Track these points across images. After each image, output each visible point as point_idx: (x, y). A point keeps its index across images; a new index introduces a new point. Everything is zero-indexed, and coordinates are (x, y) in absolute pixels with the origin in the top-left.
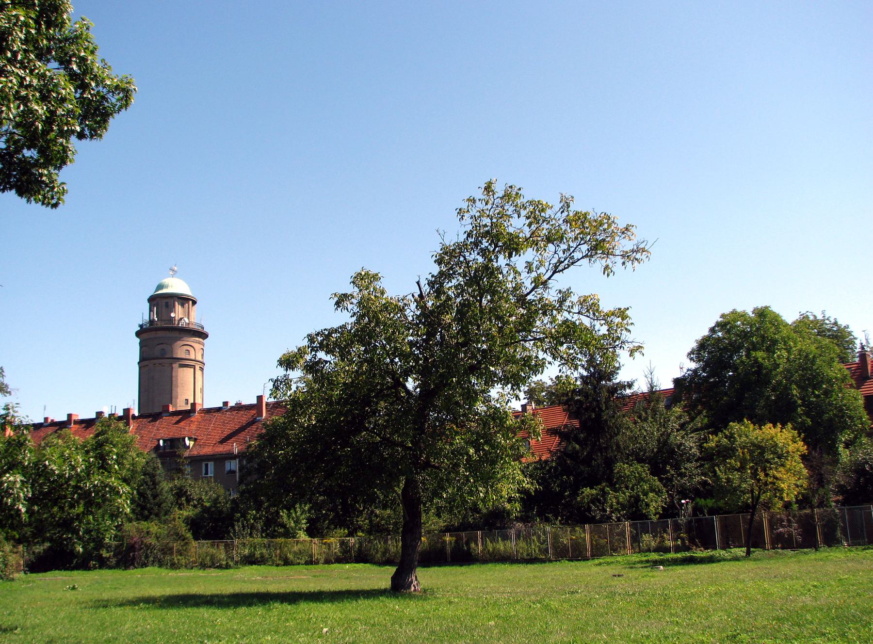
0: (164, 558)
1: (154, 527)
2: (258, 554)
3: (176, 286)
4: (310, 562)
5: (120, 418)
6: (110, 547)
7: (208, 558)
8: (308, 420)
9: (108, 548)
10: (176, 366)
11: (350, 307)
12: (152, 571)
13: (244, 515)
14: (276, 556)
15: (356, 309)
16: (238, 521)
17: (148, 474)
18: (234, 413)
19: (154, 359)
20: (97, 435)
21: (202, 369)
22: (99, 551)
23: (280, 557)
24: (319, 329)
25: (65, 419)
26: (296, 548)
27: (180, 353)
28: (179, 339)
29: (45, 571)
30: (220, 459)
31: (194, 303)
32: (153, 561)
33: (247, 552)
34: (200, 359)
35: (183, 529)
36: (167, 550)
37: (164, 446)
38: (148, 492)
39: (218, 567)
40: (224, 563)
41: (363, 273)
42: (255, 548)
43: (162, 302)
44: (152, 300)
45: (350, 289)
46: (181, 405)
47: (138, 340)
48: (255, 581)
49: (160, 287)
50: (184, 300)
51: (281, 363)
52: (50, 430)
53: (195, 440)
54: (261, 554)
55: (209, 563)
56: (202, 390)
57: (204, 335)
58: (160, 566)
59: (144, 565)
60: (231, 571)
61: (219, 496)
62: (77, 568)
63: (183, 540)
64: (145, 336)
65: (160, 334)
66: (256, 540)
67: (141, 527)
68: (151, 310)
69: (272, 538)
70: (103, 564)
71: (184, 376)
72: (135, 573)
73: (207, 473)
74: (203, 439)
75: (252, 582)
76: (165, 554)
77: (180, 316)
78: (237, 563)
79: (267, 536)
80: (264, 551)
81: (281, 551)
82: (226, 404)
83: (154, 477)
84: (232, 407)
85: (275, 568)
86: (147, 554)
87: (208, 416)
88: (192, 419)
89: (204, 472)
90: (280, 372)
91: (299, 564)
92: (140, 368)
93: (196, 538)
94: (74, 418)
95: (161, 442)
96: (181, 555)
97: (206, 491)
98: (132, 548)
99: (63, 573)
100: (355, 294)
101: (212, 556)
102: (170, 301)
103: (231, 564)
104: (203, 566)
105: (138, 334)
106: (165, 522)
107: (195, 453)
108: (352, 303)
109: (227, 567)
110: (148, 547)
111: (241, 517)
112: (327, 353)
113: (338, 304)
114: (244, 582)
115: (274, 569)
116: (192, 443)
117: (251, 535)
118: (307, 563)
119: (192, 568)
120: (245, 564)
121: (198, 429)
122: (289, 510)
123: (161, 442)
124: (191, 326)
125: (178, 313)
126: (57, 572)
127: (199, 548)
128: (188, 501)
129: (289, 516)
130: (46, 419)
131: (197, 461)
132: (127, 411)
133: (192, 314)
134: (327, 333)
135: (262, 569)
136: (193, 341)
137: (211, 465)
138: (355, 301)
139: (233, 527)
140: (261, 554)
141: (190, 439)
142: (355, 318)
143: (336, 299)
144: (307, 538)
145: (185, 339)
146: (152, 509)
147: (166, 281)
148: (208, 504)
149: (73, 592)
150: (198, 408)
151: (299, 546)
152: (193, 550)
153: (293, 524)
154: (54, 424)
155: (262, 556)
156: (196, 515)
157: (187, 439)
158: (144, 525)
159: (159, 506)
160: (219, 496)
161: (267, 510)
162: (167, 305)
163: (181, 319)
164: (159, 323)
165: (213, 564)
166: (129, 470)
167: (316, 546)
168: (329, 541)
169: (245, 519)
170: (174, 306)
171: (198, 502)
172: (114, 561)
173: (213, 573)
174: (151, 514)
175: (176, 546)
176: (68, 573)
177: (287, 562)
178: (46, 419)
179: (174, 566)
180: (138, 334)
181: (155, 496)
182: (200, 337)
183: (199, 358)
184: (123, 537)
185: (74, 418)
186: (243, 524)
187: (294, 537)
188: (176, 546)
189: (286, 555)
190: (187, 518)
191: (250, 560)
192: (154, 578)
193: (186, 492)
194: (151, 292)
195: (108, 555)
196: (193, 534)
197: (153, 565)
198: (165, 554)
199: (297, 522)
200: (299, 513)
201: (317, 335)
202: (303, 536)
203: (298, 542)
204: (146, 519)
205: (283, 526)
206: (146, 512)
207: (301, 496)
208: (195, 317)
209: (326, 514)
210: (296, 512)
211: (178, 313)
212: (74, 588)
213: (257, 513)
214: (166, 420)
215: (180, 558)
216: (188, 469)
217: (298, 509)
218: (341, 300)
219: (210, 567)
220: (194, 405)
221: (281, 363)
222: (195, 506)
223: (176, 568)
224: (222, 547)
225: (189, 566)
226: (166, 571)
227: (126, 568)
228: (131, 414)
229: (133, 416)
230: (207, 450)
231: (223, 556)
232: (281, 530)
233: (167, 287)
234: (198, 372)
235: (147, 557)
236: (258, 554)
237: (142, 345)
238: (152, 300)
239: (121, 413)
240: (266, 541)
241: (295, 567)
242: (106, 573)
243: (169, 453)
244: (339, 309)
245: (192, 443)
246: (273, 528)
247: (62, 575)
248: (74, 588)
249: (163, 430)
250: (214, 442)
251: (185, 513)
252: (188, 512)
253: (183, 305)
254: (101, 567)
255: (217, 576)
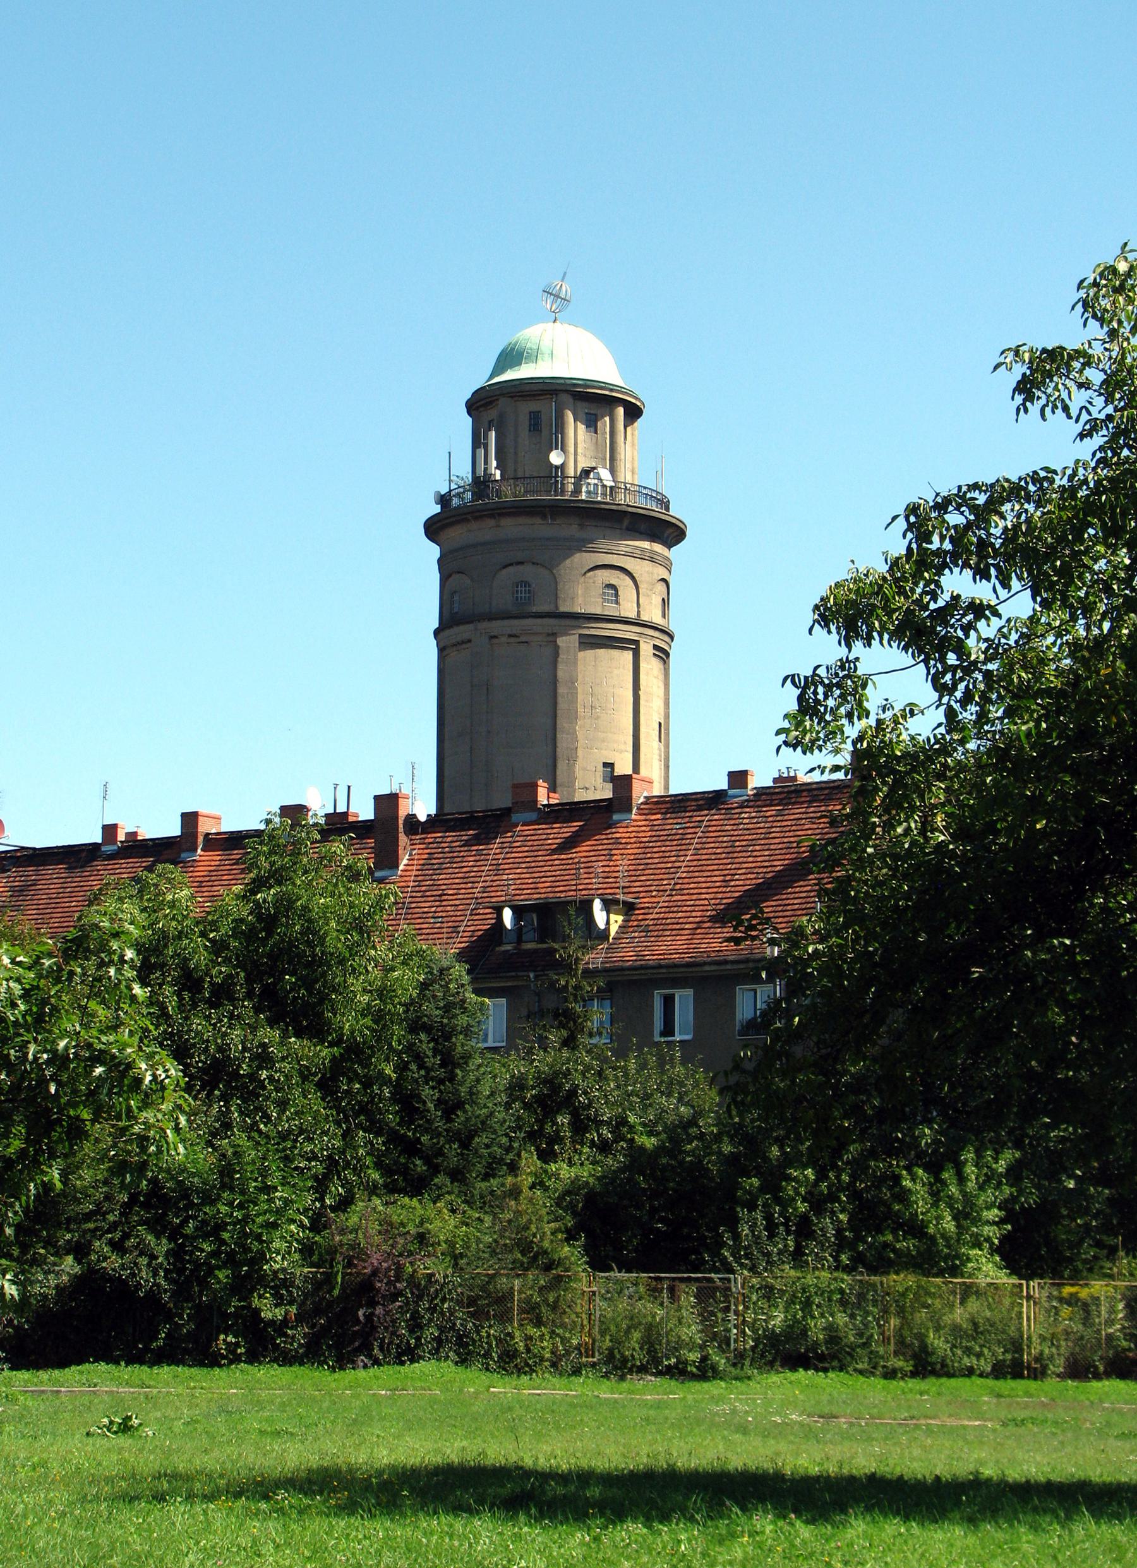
0: (478, 1329)
1: (442, 1218)
2: (816, 1328)
3: (568, 352)
4: (1015, 1367)
5: (363, 829)
6: (287, 1284)
7: (636, 1335)
8: (931, 825)
9: (280, 1287)
10: (567, 642)
11: (1079, 398)
12: (433, 1376)
13: (774, 1180)
14: (886, 1341)
15: (1100, 408)
16: (752, 1207)
17: (427, 1029)
18: (771, 811)
19: (491, 617)
20: (259, 884)
21: (662, 654)
22: (246, 1298)
23: (901, 1343)
24: (947, 487)
25: (174, 829)
26: (959, 1315)
27: (584, 596)
28: (581, 545)
29: (63, 1364)
30: (713, 980)
31: (634, 412)
32: (439, 1341)
33: (778, 1319)
34: (656, 618)
35: (546, 1232)
36: (488, 1303)
37: (518, 930)
38: (426, 1092)
39: (669, 1372)
40: (694, 1356)
41: (1123, 267)
42: (807, 1304)
43: (517, 410)
44: (482, 405)
45: (1074, 332)
46: (591, 787)
47: (434, 551)
48: (780, 1431)
49: (510, 356)
50: (596, 402)
51: (825, 615)
52: (126, 868)
53: (629, 909)
54: (830, 1328)
55: (640, 1357)
56: (663, 729)
57: (669, 532)
58: (464, 1361)
59: (408, 1354)
60: (715, 1388)
61: (699, 1113)
62: (169, 1356)
63: (548, 1268)
64: (457, 534)
65: (511, 527)
66: (810, 1280)
67: (397, 1215)
68: (478, 442)
69: (873, 1270)
70: (261, 1344)
71: (601, 681)
72: (368, 1382)
73: (668, 1030)
74: (655, 903)
75: (770, 1432)
76: (479, 1315)
77: (583, 463)
78: (740, 1356)
79: (858, 1260)
80: (841, 1319)
81: (906, 1323)
82: (738, 778)
83: (448, 1038)
84: (761, 792)
85: (878, 1383)
86: (416, 1316)
87: (674, 824)
88: (620, 833)
89: (658, 1024)
90: (827, 649)
91: (970, 1372)
92: (441, 650)
93: (598, 1264)
94: (205, 827)
95: (507, 915)
96: (538, 1322)
97: (656, 1093)
98: (364, 1290)
99: (126, 1372)
100: (1097, 350)
101: (650, 1327)
102: (547, 408)
103: (720, 1361)
104: (618, 1366)
105: (433, 529)
106: (489, 1203)
107: (627, 955)
108: (1084, 385)
109: (705, 1372)
110: (421, 1288)
111: (763, 1189)
112: (982, 573)
113: (1026, 388)
114: (744, 1429)
115: (875, 1389)
116: (617, 920)
117: (797, 1257)
118: (999, 1371)
119: (577, 1372)
120: (771, 1364)
121: (639, 868)
122: (934, 1169)
123: (507, 915)
124: (621, 498)
125: (576, 449)
126: (102, 1366)
127: (603, 1298)
128: (580, 1127)
129: (936, 1194)
130: (110, 830)
131: (630, 986)
132: (387, 803)
133: (628, 452)
134: (982, 499)
135: (829, 1386)
136: (630, 551)
137: (684, 998)
138: (1096, 377)
139: (733, 1223)
140: (830, 1328)
141: (609, 905)
142: (1098, 440)
143: (1020, 370)
144: (1004, 1279)
145: (603, 544)
146: (440, 1153)
147: (533, 335)
148: (649, 1142)
149: (123, 1441)
150: (639, 794)
151: (973, 1305)
152: (581, 1305)
153: (949, 1225)
154: (137, 847)
155: (833, 1336)
156: (609, 1180)
157: (597, 904)
158: (409, 1210)
159: (465, 1144)
160: (699, 1113)
161: (859, 1167)
162: (535, 423)
163: (586, 473)
164: (507, 489)
165: (656, 1361)
166: (366, 1011)
167: (1035, 1311)
168: (1084, 1294)
169: (778, 1200)
170: (561, 427)
171: (615, 1131)
172: (299, 1335)
173: (651, 1390)
174: (435, 1170)
175: (521, 1287)
176: (141, 1372)
177: (925, 1365)
178: (110, 830)
179: (512, 1362)
180: (433, 529)
181: (450, 1107)
182: (653, 537)
183: (653, 614)
184: (332, 1251)
185: (205, 827)
186: (769, 1217)
187: (954, 1271)
188: (521, 1287)
189: (921, 1338)
190: (574, 1188)
191: (790, 1352)
192: (433, 1401)
193: (573, 1093)
194: (478, 378)
195: (279, 1313)
196: (588, 1249)
197: (436, 1353)
198: (479, 1315)
199: (965, 1215)
200: (971, 1185)
201: (942, 506)
202: (987, 1270)
203: (968, 1291)
204: (416, 1187)
205: (916, 1229)
206: (419, 1165)
207: (969, 1124)
208: (639, 464)
209: (1079, 1191)
210: (962, 1179)
211: (576, 449)
212: (126, 1427)
213: (821, 1176)
214: (526, 835)
215: (532, 1331)
216: (598, 1015)
217: (970, 1170)
218: (1041, 374)
219: (642, 1369)
220: (623, 784)
221: (825, 615)
222: (604, 1147)
223: (520, 1371)
224: (688, 1298)
225: (566, 1364)
226: (485, 1378)
227: (343, 1361)
228: (402, 814)
229: (411, 819)
230: (670, 948)
231: (692, 1331)
232: (907, 1244)
233: (533, 356)
234: (650, 666)
235: (416, 1326)
236: (816, 1328)
237: (449, 568)
238: (482, 405)
239: (365, 811)
240: (846, 1281)
241: (953, 1382)
242: (269, 1377)
243: (527, 957)
244: (1034, 408)
245: (617, 920)
246: (880, 1238)
247: (119, 1382)
248: (126, 1427)
249: (511, 875)
250: (697, 916)
251: (564, 1171)
252: (573, 1169)
253: (591, 423)
254: (253, 1358)
255: (658, 1405)
